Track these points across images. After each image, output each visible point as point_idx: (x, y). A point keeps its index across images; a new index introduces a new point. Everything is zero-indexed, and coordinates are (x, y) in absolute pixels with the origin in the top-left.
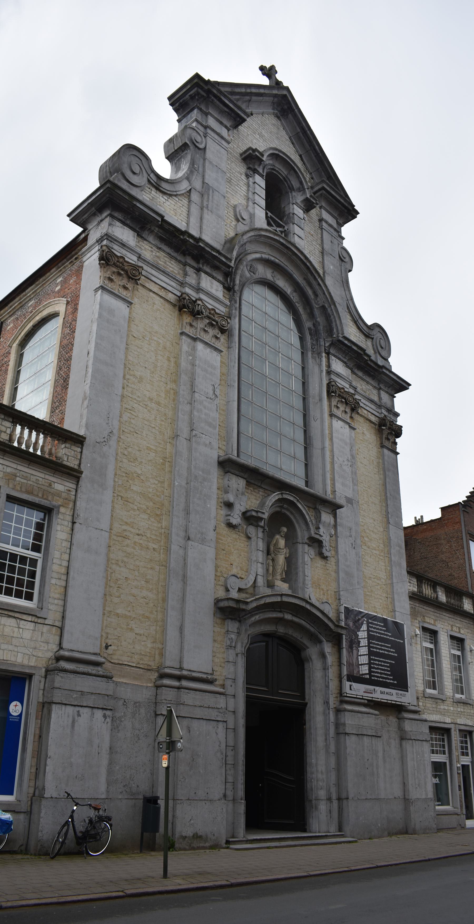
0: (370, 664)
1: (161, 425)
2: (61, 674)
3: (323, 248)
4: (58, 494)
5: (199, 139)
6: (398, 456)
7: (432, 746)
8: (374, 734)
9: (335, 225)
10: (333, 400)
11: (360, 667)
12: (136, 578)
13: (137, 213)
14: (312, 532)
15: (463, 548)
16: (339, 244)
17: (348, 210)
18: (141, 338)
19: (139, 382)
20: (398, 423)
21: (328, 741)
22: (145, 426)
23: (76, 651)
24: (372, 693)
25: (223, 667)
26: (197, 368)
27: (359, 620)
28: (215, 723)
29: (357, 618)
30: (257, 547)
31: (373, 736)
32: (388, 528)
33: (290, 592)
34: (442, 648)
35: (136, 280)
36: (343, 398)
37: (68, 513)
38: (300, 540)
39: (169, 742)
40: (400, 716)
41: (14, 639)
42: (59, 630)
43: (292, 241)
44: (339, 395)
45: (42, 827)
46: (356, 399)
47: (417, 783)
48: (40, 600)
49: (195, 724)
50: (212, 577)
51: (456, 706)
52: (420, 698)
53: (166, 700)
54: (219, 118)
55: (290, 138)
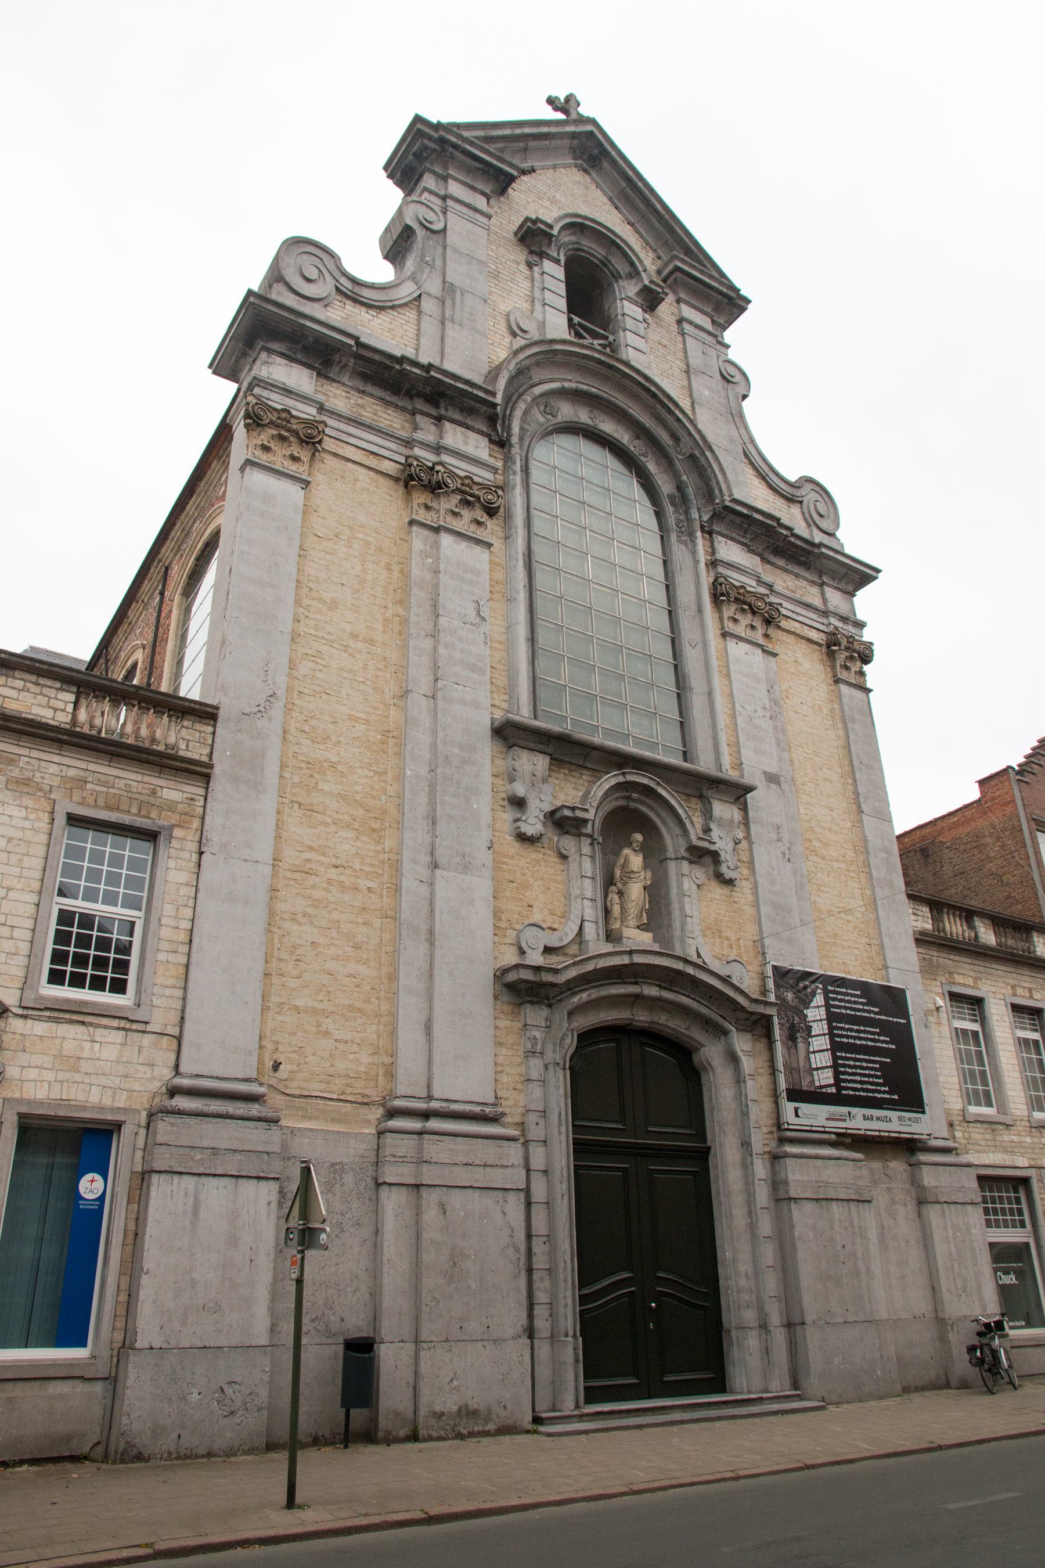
0: (835, 1066)
1: (377, 677)
2: (171, 1119)
3: (688, 365)
4: (171, 807)
5: (431, 216)
6: (871, 694)
7: (986, 1211)
8: (853, 1197)
9: (709, 326)
10: (724, 609)
11: (815, 1073)
12: (333, 941)
13: (311, 339)
14: (693, 838)
15: (1024, 846)
16: (718, 356)
17: (730, 298)
18: (332, 537)
19: (330, 609)
20: (864, 639)
21: (754, 1215)
22: (344, 681)
23: (207, 1077)
24: (845, 1120)
25: (521, 1091)
26: (441, 575)
27: (805, 988)
28: (500, 1194)
29: (801, 985)
30: (581, 871)
31: (852, 1200)
32: (861, 821)
33: (656, 948)
34: (996, 1028)
35: (314, 443)
36: (745, 603)
37: (189, 838)
38: (671, 853)
39: (303, 1230)
40: (914, 1159)
41: (82, 1062)
42: (175, 1042)
43: (624, 357)
44: (737, 600)
45: (129, 1406)
46: (771, 604)
47: (959, 1286)
48: (139, 992)
49: (456, 1198)
50: (489, 931)
51: (1038, 1134)
52: (956, 1123)
53: (394, 1156)
54: (468, 181)
55: (610, 199)
